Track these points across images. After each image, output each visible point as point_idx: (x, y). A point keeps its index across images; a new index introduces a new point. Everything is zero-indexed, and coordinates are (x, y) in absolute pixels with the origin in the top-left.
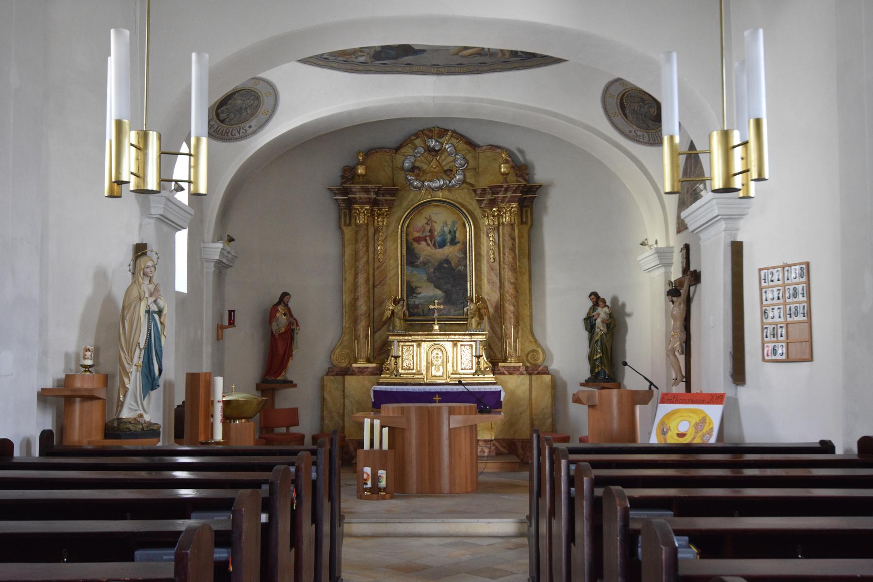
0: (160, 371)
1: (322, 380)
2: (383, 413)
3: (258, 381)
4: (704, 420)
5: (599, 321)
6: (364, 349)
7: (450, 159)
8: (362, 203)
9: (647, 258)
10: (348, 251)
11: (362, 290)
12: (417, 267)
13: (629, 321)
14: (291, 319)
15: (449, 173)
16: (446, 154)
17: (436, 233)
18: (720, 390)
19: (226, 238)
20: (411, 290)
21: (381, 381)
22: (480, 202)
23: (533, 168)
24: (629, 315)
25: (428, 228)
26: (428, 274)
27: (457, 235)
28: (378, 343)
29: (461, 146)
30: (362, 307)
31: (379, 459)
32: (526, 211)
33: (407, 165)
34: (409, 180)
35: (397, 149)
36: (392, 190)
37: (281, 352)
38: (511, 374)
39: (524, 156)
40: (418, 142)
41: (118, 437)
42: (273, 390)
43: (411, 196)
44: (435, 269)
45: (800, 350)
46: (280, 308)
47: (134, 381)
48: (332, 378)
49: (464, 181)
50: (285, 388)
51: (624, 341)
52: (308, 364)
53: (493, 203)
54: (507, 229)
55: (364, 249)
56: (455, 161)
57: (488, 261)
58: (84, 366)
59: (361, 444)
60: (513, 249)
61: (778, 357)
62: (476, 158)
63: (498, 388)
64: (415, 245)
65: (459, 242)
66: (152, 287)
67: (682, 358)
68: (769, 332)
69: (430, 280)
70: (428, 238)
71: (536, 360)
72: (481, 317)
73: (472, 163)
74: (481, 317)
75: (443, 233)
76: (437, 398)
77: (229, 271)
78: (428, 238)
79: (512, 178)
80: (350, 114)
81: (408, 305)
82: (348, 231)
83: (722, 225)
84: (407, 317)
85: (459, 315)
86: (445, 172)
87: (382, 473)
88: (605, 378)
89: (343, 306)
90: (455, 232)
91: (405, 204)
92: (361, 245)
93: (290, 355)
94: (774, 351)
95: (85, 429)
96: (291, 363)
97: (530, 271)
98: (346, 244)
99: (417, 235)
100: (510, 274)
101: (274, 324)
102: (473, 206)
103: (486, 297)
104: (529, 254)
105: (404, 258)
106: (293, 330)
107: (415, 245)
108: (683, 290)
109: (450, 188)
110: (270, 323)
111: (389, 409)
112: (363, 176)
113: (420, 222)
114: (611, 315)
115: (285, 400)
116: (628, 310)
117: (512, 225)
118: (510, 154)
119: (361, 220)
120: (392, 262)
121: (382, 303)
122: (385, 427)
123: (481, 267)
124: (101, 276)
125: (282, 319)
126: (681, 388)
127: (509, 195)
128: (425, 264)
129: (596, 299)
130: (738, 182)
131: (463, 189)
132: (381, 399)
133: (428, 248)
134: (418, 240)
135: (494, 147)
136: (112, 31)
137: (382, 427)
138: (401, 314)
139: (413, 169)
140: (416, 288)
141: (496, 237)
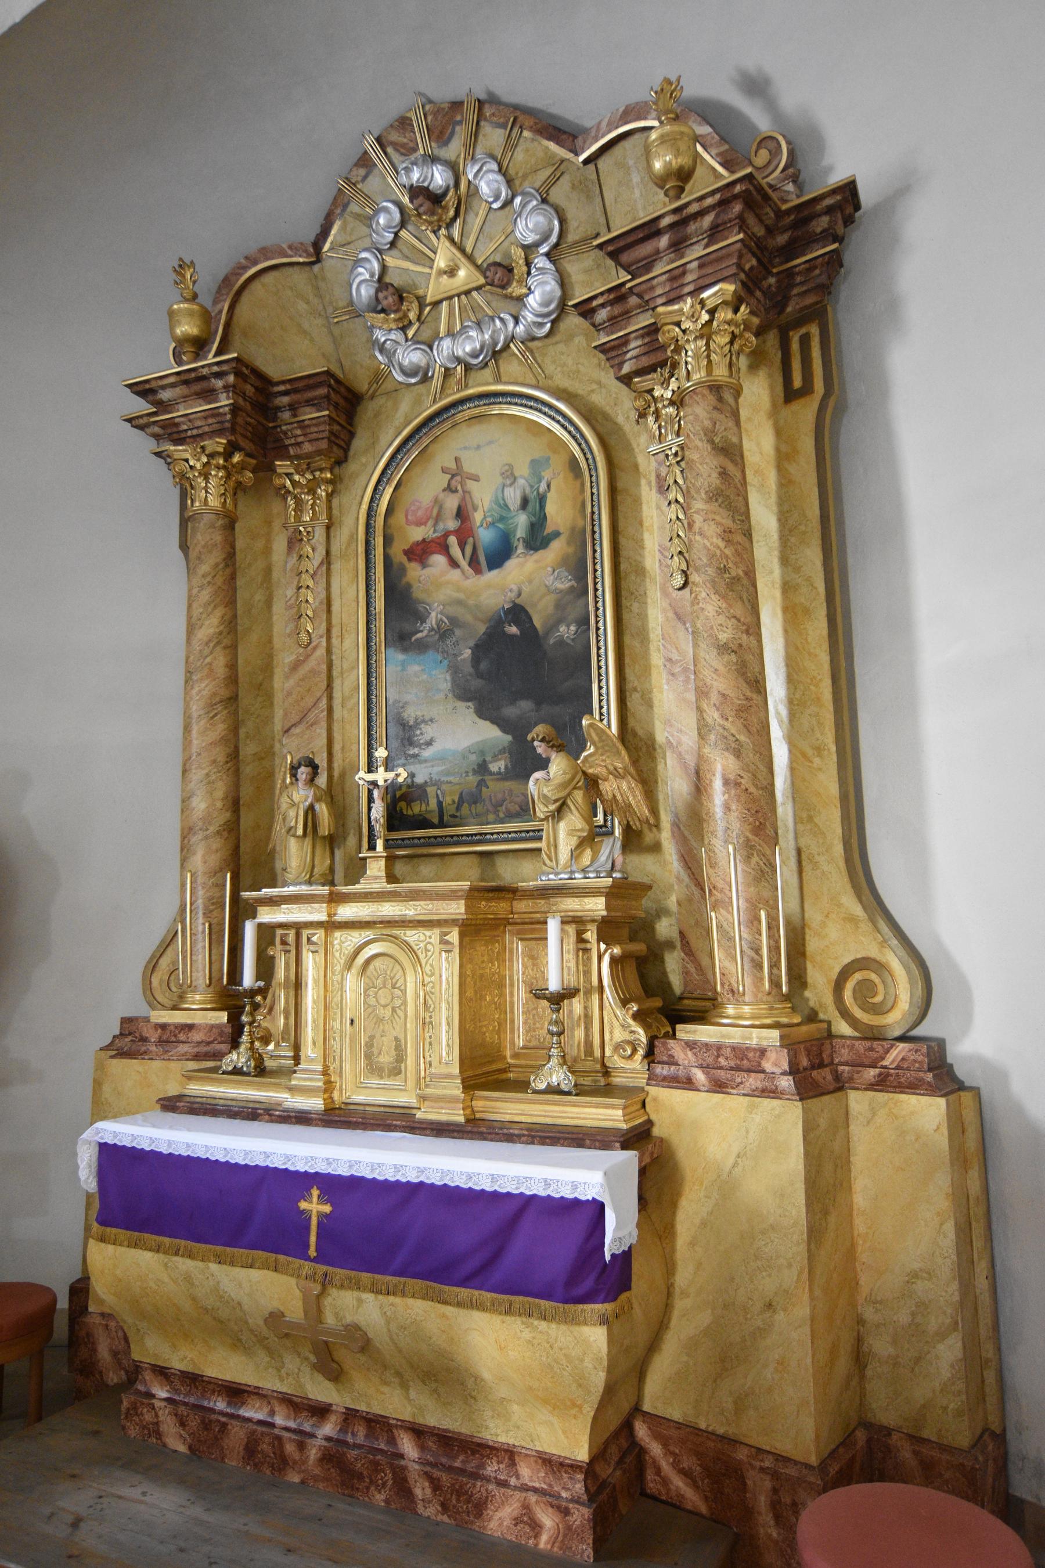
12: (422, 647)
15: (501, 276)
17: (478, 517)
25: (452, 503)
26: (455, 670)
27: (550, 508)
32: (805, 340)
38: (719, 1087)
39: (771, 106)
43: (405, 406)
65: (557, 534)
69: (463, 693)
70: (452, 540)
71: (878, 1010)
75: (502, 515)
78: (452, 540)
90: (542, 499)
99: (418, 534)
105: (380, 623)
107: (414, 572)
113: (428, 488)
128: (443, 633)
131: (570, 337)
133: (455, 574)
134: (420, 553)
140: (417, 724)
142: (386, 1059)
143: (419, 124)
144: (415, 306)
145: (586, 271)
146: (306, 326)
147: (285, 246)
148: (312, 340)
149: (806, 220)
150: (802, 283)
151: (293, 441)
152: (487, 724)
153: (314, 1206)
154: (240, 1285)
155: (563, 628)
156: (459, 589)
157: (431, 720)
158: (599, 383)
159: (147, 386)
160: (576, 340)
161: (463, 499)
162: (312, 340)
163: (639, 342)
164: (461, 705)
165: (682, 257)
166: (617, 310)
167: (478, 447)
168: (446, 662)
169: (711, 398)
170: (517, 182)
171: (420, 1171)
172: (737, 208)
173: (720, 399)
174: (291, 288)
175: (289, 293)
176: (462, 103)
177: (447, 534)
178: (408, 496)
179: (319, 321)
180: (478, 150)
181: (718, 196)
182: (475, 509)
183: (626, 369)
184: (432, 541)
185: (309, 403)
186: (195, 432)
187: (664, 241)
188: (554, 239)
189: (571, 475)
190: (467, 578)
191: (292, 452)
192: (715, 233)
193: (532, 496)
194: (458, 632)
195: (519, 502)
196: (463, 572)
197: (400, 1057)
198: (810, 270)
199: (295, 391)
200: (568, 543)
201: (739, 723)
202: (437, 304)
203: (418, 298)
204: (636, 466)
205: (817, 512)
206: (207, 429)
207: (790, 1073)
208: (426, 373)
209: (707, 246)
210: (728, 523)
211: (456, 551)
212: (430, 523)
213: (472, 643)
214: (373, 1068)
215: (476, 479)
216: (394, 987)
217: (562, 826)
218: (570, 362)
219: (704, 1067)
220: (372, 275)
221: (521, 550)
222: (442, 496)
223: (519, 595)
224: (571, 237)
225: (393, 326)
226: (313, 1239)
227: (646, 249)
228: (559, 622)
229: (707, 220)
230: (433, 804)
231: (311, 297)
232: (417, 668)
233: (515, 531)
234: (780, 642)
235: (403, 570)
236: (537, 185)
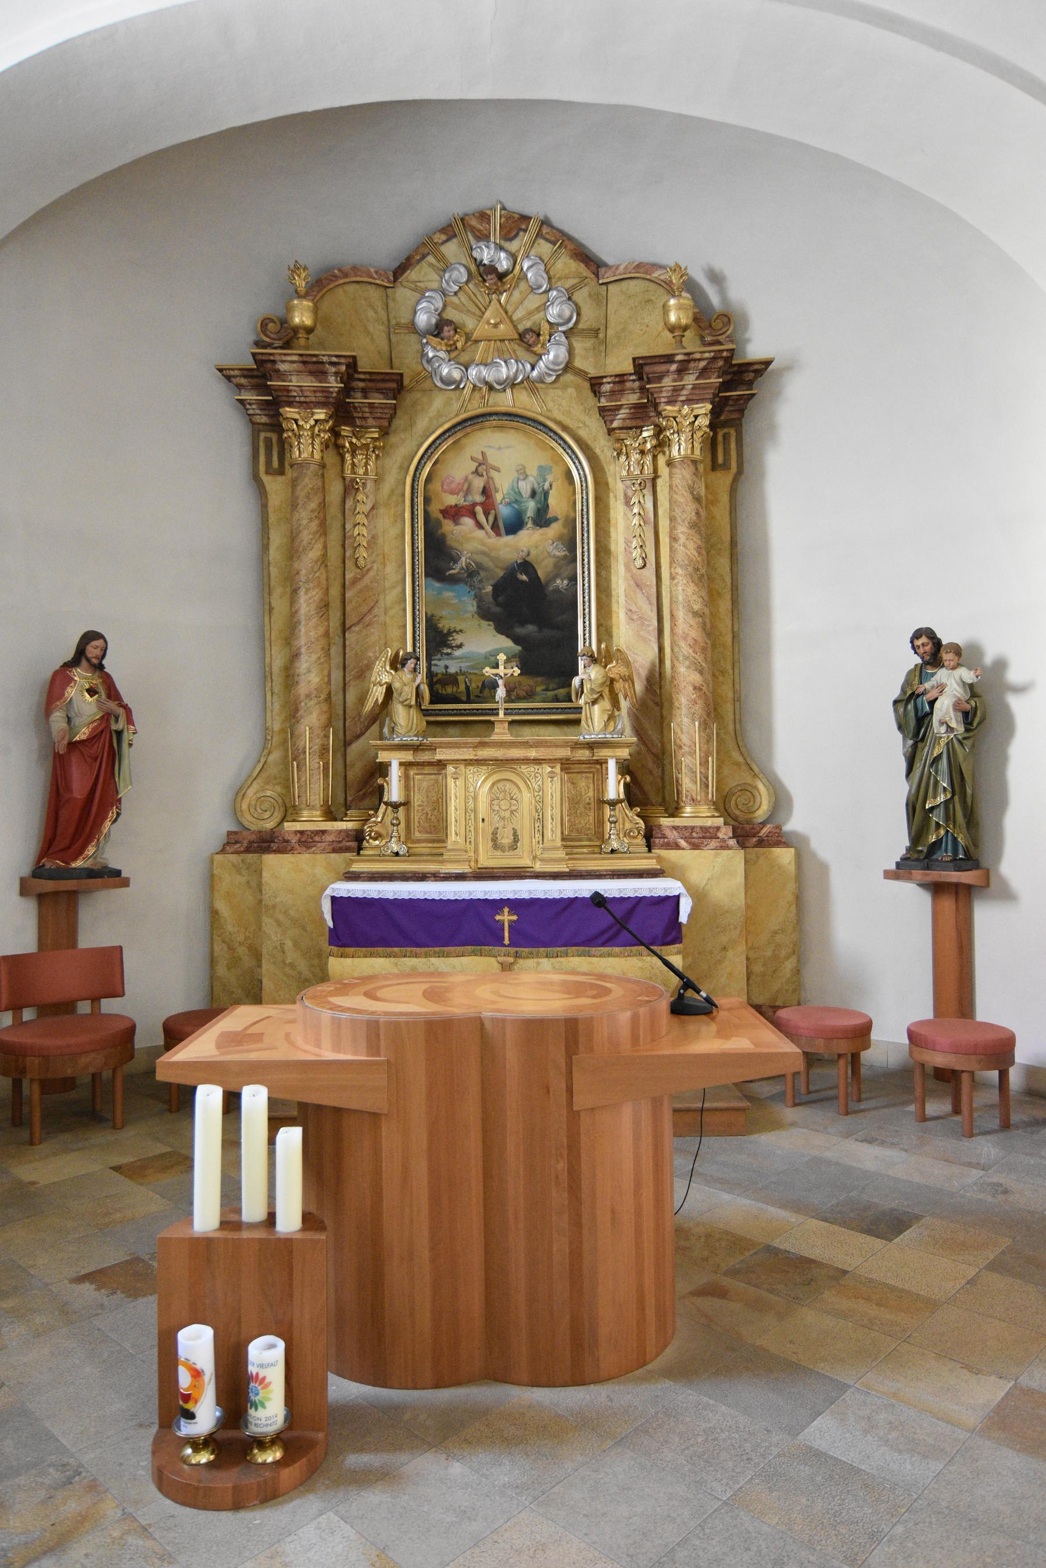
0: (979, 724)
3: (26, 870)
6: (314, 787)
7: (533, 302)
10: (277, 539)
11: (309, 633)
12: (453, 580)
13: (1014, 702)
14: (112, 705)
15: (529, 340)
16: (523, 285)
17: (499, 497)
20: (438, 639)
21: (357, 867)
23: (744, 322)
25: (479, 483)
26: (479, 598)
27: (552, 501)
28: (355, 773)
29: (565, 264)
30: (310, 675)
32: (726, 437)
33: (423, 319)
34: (429, 361)
35: (400, 271)
36: (385, 377)
38: (695, 847)
40: (451, 249)
42: (72, 898)
43: (438, 402)
44: (496, 587)
46: (81, 676)
48: (234, 858)
49: (568, 367)
50: (106, 887)
51: (1003, 760)
54: (683, 475)
55: (314, 525)
56: (544, 307)
57: (627, 567)
62: (601, 301)
64: (448, 526)
65: (556, 519)
69: (484, 614)
70: (479, 509)
73: (590, 316)
75: (516, 499)
78: (479, 509)
79: (691, 343)
81: (430, 675)
82: (275, 486)
84: (426, 705)
85: (556, 699)
87: (266, 1355)
88: (954, 860)
89: (266, 676)
90: (546, 494)
91: (422, 423)
92: (304, 515)
97: (735, 588)
98: (272, 518)
99: (451, 500)
100: (691, 588)
101: (58, 719)
102: (592, 429)
104: (733, 543)
105: (421, 559)
106: (119, 733)
107: (448, 526)
109: (532, 385)
112: (309, 330)
113: (459, 468)
116: (1014, 676)
118: (690, 286)
119: (306, 449)
120: (390, 568)
121: (364, 672)
122: (290, 1122)
123: (608, 580)
127: (690, 380)
128: (471, 574)
129: (932, 650)
131: (565, 387)
133: (480, 534)
134: (454, 513)
135: (643, 270)
139: (438, 329)
141: (649, 505)
142: (506, 840)
143: (497, 221)
144: (463, 339)
145: (585, 349)
146: (371, 329)
147: (372, 270)
148: (372, 339)
149: (741, 373)
150: (732, 405)
151: (360, 415)
152: (503, 637)
153: (506, 917)
154: (454, 967)
155: (558, 581)
156: (484, 544)
157: (461, 631)
158: (584, 423)
159: (272, 358)
160: (570, 390)
161: (488, 482)
162: (372, 339)
163: (627, 411)
164: (484, 623)
165: (681, 380)
166: (617, 388)
167: (500, 448)
168: (473, 593)
169: (692, 468)
170: (553, 281)
171: (575, 891)
172: (721, 363)
173: (697, 469)
174: (366, 300)
175: (364, 302)
176: (531, 218)
177: (475, 505)
178: (443, 472)
179: (382, 328)
180: (532, 252)
181: (712, 354)
182: (497, 491)
183: (615, 424)
184: (463, 507)
185: (379, 390)
186: (302, 399)
187: (674, 367)
188: (571, 325)
189: (566, 483)
190: (490, 537)
191: (358, 422)
192: (703, 373)
193: (539, 490)
194: (482, 574)
195: (529, 492)
196: (487, 533)
197: (516, 839)
198: (738, 400)
199: (370, 380)
200: (564, 526)
201: (702, 656)
202: (477, 342)
203: (466, 334)
204: (607, 484)
205: (729, 539)
206: (313, 399)
207: (734, 837)
208: (458, 386)
209: (697, 379)
210: (699, 542)
211: (481, 517)
212: (461, 494)
213: (493, 582)
214: (496, 846)
215: (498, 470)
216: (512, 799)
217: (596, 707)
218: (564, 403)
219: (685, 838)
220: (436, 310)
221: (530, 524)
222: (471, 477)
223: (528, 554)
224: (580, 326)
225: (444, 348)
226: (506, 934)
227: (663, 368)
228: (555, 577)
229: (702, 364)
230: (462, 687)
231: (380, 309)
232: (451, 594)
233: (526, 511)
235: (439, 524)
236: (567, 286)
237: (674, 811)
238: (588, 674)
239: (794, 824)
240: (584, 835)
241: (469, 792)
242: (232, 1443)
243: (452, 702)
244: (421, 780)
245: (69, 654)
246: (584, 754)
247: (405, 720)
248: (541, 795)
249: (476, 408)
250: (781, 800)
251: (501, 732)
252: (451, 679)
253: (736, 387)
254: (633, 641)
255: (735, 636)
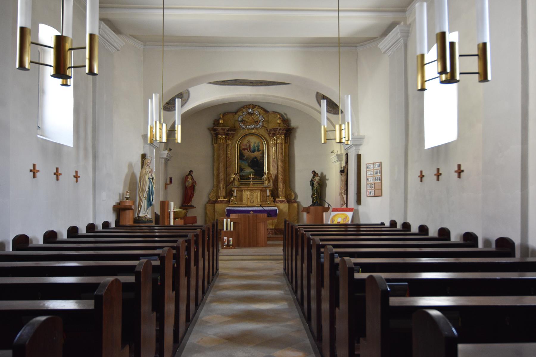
1: (206, 205)
2: (231, 217)
4: (346, 217)
5: (315, 182)
6: (222, 193)
7: (257, 117)
8: (222, 135)
9: (333, 158)
10: (216, 154)
12: (244, 160)
13: (327, 182)
15: (257, 122)
18: (352, 207)
19: (168, 149)
22: (269, 134)
23: (290, 121)
24: (327, 180)
25: (248, 144)
27: (260, 147)
29: (261, 111)
30: (222, 176)
31: (229, 234)
35: (236, 113)
37: (190, 194)
40: (244, 110)
41: (139, 223)
43: (242, 131)
45: (378, 193)
47: (144, 203)
49: (263, 126)
52: (200, 199)
53: (274, 135)
56: (259, 118)
58: (127, 198)
59: (223, 230)
60: (282, 153)
61: (372, 195)
63: (276, 208)
64: (243, 151)
66: (150, 170)
67: (345, 196)
68: (369, 186)
69: (249, 166)
72: (269, 181)
73: (266, 119)
74: (269, 181)
76: (252, 212)
77: (169, 162)
79: (282, 125)
80: (218, 100)
82: (215, 145)
83: (354, 148)
86: (255, 122)
87: (231, 239)
91: (239, 135)
93: (193, 196)
94: (370, 193)
95: (128, 219)
96: (194, 199)
99: (244, 147)
101: (187, 183)
103: (271, 173)
104: (289, 155)
107: (243, 151)
108: (344, 171)
109: (257, 129)
110: (185, 182)
111: (233, 216)
113: (245, 142)
114: (320, 180)
115: (191, 213)
116: (327, 178)
117: (282, 144)
118: (281, 115)
119: (221, 141)
120: (234, 158)
121: (230, 175)
124: (130, 166)
125: (190, 181)
126: (345, 207)
127: (281, 132)
128: (247, 159)
129: (315, 173)
130: (343, 140)
132: (229, 212)
134: (244, 149)
135: (275, 112)
136: (154, 94)
137: (231, 222)
138: (237, 179)
139: (242, 121)
192: (283, 130)
234: (328, 282)
237: (279, 197)
238: (265, 176)
239: (298, 200)
240: (264, 201)
241: (246, 194)
242: (228, 245)
243: (244, 180)
244: (239, 192)
245: (188, 173)
246: (264, 189)
247: (236, 183)
248: (257, 195)
249: (249, 132)
250: (296, 196)
251: (251, 186)
252: (243, 176)
253: (288, 132)
254: (273, 171)
255: (289, 169)
